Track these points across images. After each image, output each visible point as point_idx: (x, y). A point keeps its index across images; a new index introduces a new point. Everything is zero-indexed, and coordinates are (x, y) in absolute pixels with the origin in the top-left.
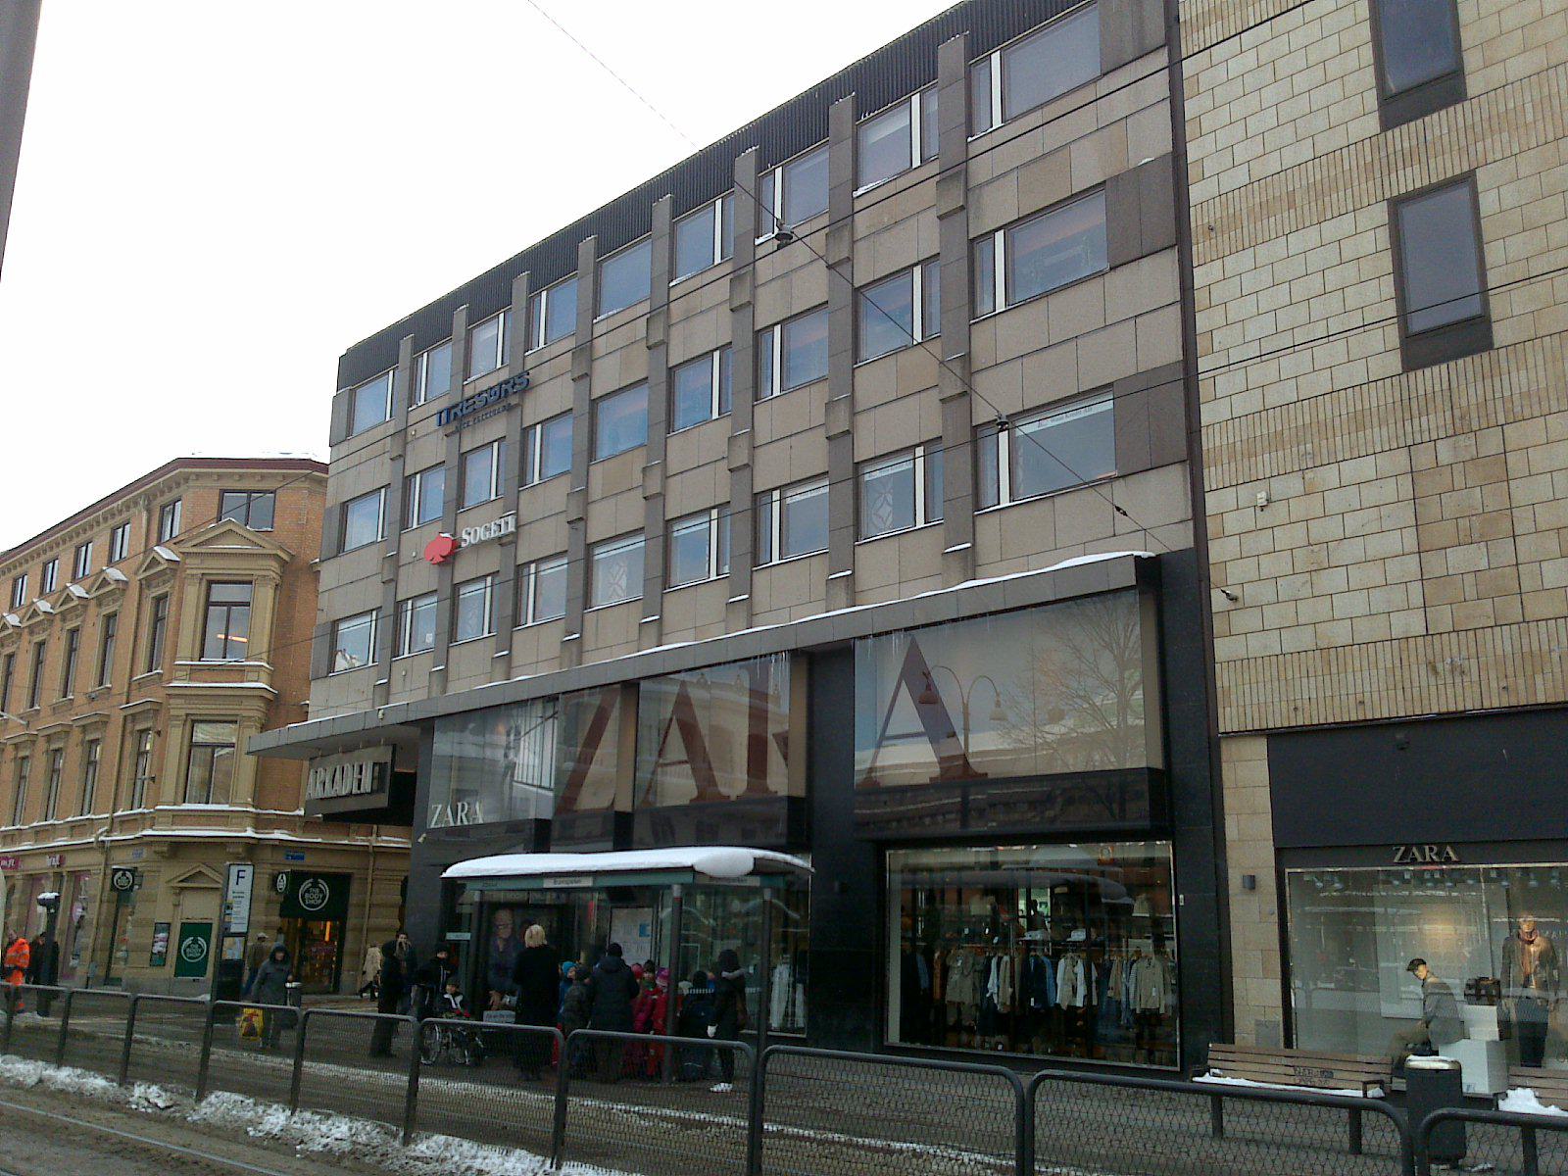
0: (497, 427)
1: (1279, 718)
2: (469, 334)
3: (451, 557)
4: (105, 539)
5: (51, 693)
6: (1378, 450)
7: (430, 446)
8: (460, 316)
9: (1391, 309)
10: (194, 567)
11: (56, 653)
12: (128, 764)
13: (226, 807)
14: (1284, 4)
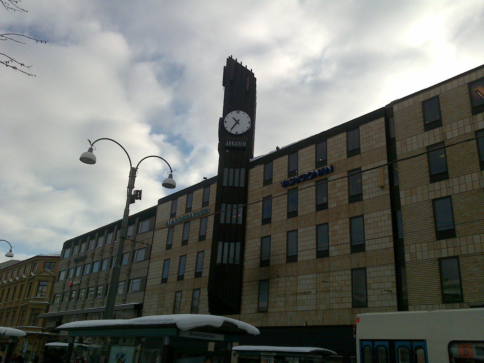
0: (81, 263)
2: (107, 236)
3: (72, 286)
4: (11, 272)
5: (10, 300)
7: (73, 265)
8: (137, 219)
9: (315, 247)
10: (37, 278)
11: (11, 292)
12: (20, 316)
13: (36, 327)
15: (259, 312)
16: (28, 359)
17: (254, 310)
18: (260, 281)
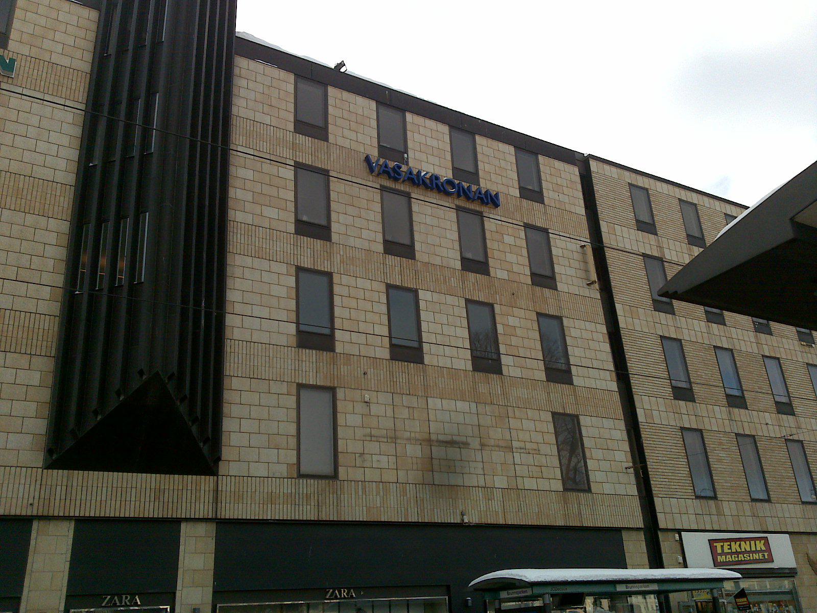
1: (91, 511)
6: (8, 312)
14: (816, 477)
15: (301, 476)
16: (618, 370)
17: (283, 470)
18: (300, 386)
